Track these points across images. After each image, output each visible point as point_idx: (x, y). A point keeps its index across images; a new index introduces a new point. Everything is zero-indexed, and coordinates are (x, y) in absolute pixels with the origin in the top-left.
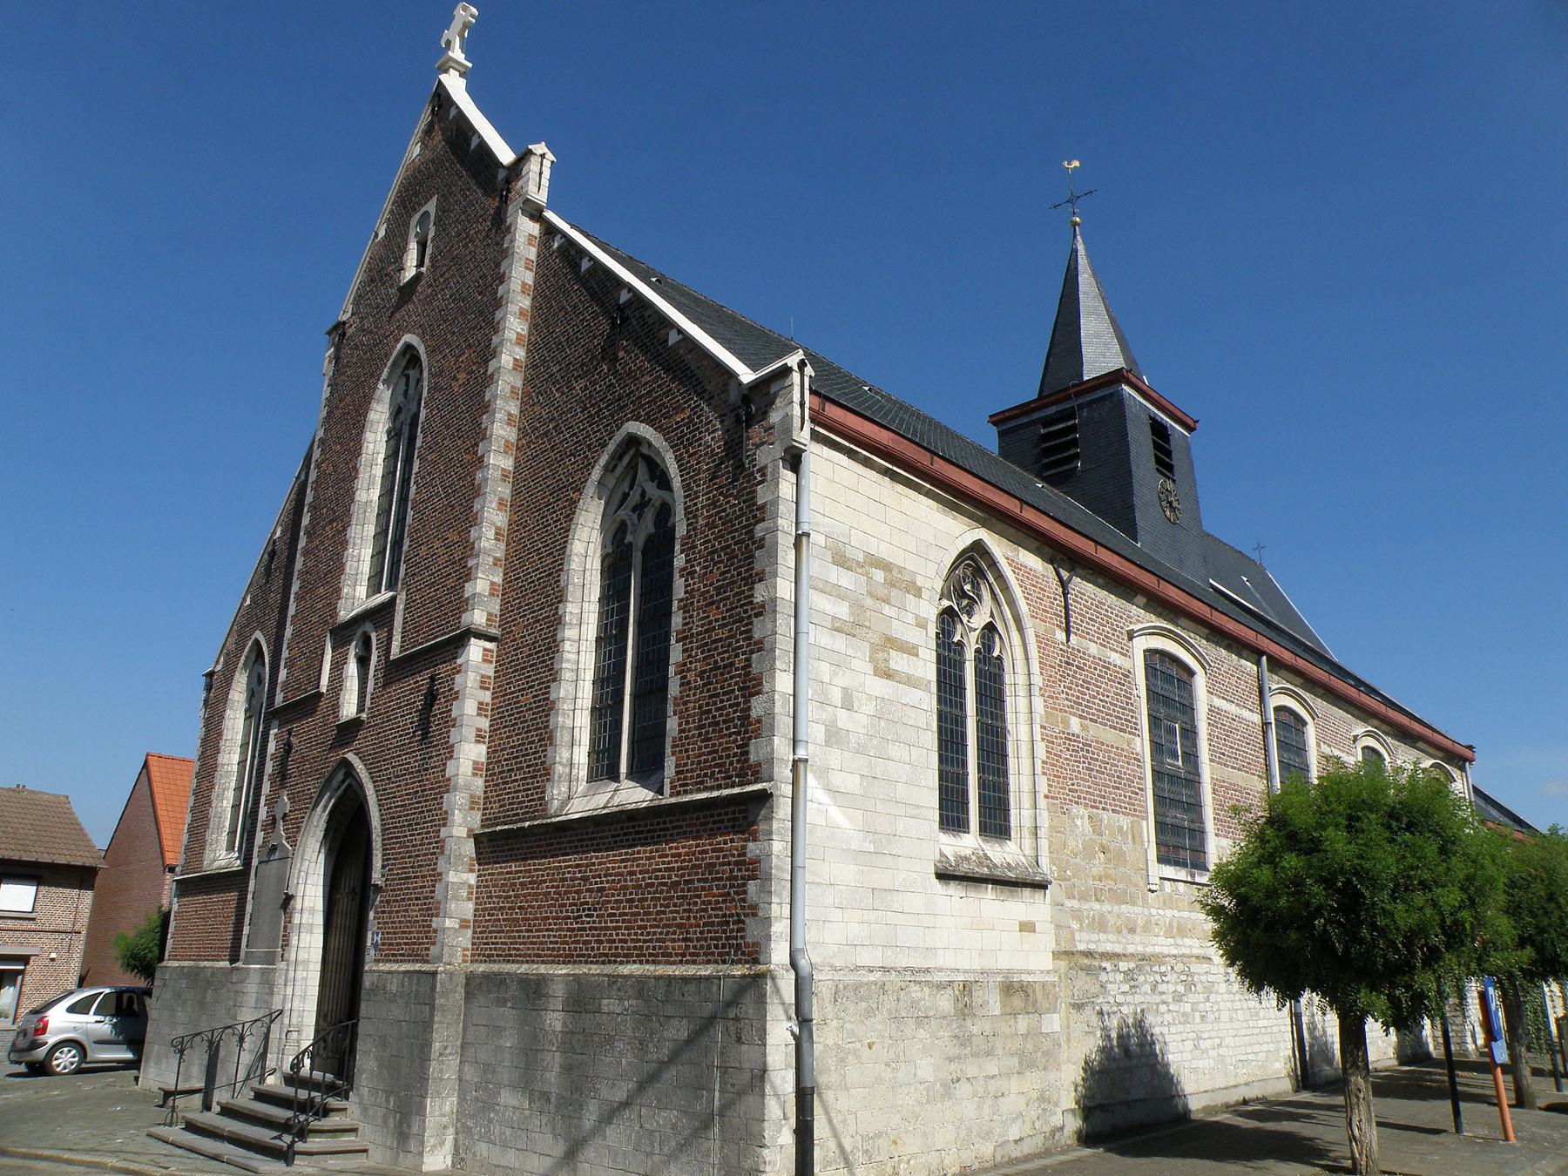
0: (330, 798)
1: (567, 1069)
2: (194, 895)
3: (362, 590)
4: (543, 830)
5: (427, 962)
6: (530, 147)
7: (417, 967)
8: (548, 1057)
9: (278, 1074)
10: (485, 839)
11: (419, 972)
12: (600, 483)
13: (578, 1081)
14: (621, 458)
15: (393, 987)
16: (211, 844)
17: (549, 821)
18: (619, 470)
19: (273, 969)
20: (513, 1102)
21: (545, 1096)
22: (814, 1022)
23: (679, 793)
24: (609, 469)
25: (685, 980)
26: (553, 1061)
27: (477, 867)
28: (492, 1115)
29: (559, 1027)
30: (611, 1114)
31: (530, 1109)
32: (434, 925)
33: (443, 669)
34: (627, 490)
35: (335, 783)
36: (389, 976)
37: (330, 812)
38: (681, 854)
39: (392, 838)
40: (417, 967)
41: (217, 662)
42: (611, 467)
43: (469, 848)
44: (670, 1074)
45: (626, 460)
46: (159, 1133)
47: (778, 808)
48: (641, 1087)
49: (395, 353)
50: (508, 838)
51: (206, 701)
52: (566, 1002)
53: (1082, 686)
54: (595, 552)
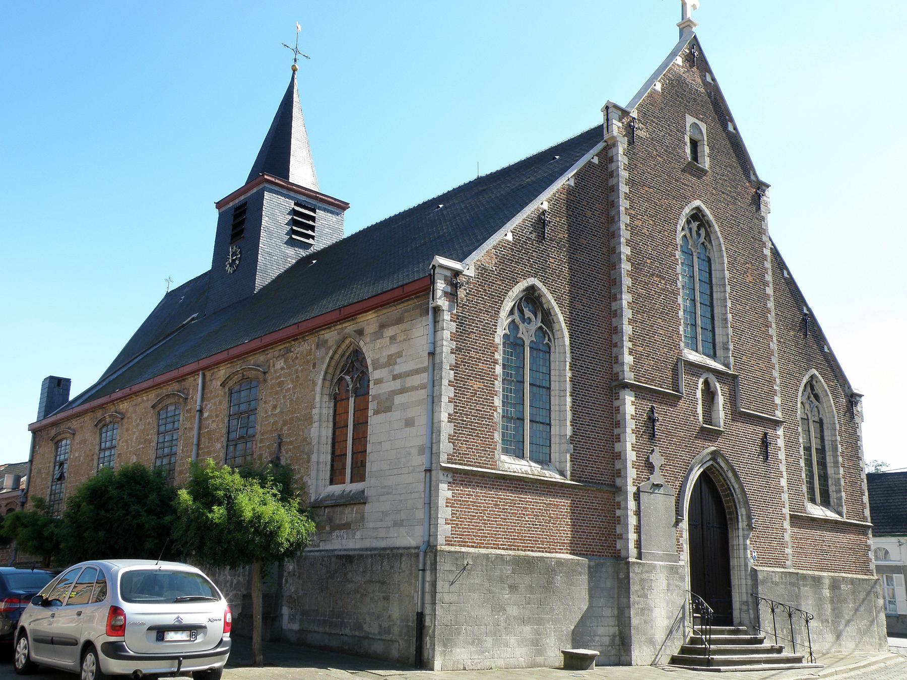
1: (833, 609)
2: (541, 495)
4: (806, 518)
5: (786, 568)
8: (826, 606)
13: (837, 614)
15: (776, 579)
20: (816, 625)
23: (848, 519)
25: (863, 580)
26: (828, 607)
30: (848, 622)
31: (822, 626)
32: (786, 552)
36: (774, 574)
39: (755, 505)
44: (862, 609)
48: (855, 613)
52: (830, 586)
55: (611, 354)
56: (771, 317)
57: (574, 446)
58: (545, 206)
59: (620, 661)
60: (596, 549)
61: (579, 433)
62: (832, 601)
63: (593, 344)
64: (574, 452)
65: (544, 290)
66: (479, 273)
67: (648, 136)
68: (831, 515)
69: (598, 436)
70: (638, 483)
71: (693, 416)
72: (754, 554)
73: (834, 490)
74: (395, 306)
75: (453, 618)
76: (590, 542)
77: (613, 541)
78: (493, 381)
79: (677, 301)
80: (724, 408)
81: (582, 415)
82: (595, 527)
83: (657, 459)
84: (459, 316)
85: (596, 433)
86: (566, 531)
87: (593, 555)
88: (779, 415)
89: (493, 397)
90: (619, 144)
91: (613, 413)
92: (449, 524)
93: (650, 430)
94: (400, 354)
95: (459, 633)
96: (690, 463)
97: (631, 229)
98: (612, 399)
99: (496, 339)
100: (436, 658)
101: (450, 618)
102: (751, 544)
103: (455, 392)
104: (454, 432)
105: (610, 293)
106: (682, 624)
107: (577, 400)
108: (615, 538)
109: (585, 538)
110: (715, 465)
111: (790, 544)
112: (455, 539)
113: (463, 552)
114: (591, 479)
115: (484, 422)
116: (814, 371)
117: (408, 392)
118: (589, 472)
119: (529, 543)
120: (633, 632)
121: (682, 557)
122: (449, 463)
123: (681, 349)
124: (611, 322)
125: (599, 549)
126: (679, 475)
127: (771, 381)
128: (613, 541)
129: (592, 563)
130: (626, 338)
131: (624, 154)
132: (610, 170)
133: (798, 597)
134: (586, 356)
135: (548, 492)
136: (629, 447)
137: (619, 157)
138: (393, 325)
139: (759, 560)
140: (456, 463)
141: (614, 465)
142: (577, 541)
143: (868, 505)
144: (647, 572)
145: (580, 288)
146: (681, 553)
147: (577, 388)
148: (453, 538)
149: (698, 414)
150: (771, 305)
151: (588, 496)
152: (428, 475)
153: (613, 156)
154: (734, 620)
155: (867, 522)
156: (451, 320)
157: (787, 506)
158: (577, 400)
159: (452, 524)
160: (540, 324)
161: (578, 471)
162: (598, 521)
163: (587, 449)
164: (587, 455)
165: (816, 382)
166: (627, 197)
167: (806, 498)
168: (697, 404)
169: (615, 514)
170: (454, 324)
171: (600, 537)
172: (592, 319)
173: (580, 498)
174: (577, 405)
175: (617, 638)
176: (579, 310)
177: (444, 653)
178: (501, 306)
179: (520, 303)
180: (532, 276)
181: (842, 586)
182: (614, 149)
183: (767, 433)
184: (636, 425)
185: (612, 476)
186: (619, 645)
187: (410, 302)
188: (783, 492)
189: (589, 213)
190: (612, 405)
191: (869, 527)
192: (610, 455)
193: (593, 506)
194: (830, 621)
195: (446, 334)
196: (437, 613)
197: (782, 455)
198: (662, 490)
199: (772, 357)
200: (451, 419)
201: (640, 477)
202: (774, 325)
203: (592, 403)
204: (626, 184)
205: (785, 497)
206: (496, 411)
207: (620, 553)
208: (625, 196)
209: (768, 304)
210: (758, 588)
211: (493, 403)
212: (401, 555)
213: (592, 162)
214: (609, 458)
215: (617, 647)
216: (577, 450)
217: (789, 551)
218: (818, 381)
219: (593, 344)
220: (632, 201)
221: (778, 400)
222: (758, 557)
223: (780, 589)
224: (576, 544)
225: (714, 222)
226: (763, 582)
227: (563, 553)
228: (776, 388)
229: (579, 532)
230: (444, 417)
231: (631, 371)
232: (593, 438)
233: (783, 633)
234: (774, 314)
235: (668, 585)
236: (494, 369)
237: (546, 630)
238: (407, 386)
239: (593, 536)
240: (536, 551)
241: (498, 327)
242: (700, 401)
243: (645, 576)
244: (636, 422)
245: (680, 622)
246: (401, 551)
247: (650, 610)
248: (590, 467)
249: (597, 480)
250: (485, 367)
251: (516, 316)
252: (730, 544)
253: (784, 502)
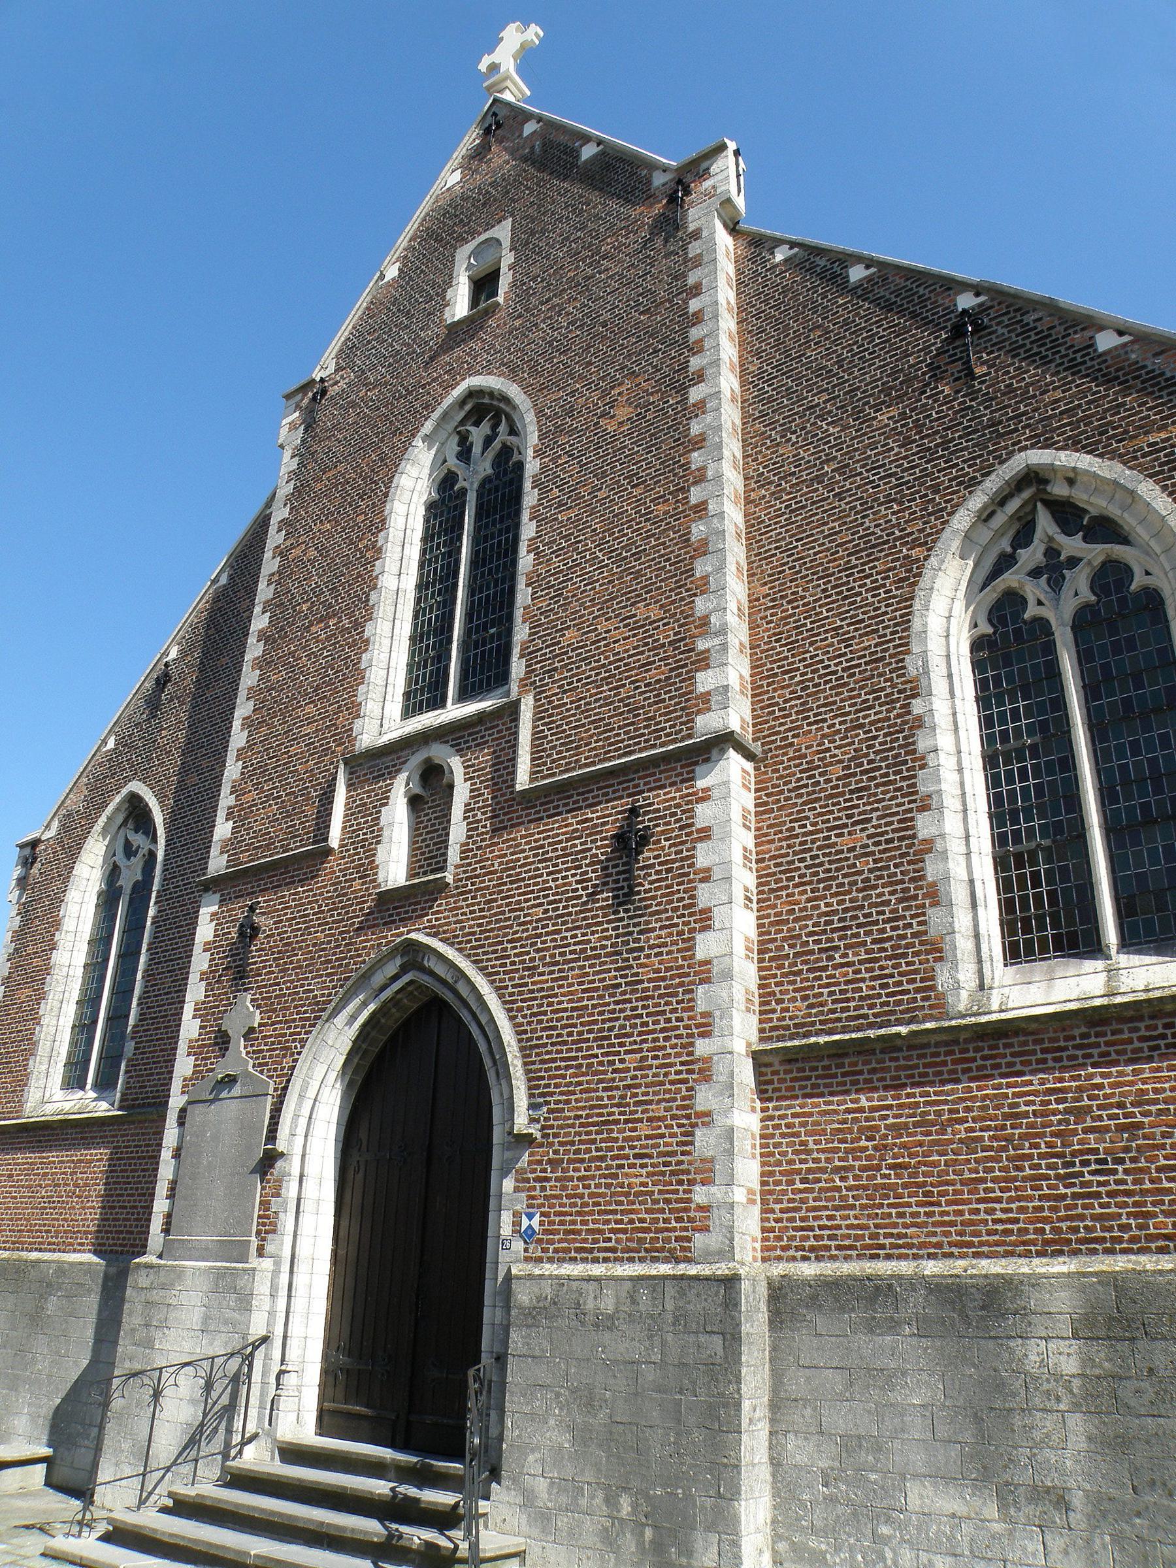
0: (365, 1004)
3: (395, 707)
5: (688, 1260)
6: (726, 140)
7: (664, 1269)
9: (263, 1443)
10: (775, 1060)
11: (682, 1277)
12: (967, 537)
14: (1002, 503)
16: (38, 1079)
17: (953, 1023)
18: (1000, 519)
19: (244, 1270)
24: (985, 517)
27: (758, 1104)
28: (885, 1530)
33: (658, 799)
34: (1009, 549)
35: (379, 979)
36: (592, 1286)
37: (364, 1026)
38: (918, 1103)
40: (664, 1269)
41: (48, 827)
42: (984, 516)
43: (745, 1073)
45: (1013, 505)
46: (85, 1554)
49: (447, 402)
50: (846, 1055)
51: (22, 882)
54: (960, 631)
72: (525, 1222)
102: (517, 1190)
106: (224, 1424)
110: (425, 979)
129: (113, 1270)
135: (82, 1138)
144: (163, 1287)
146: (269, 1237)
194: (1077, 1499)
196: (509, 1379)
198: (237, 1090)
214: (534, 1031)
222: (546, 1232)
224: (106, 1232)
235: (206, 1318)
240: (45, 1250)
243: (155, 1296)
245: (221, 1418)
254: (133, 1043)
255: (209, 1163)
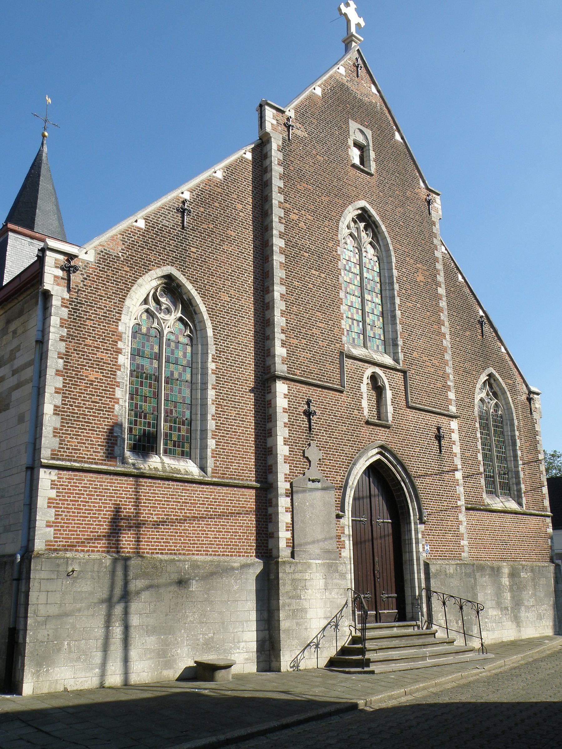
1: (513, 597)
6: (349, 1)
21: (506, 608)
22: (147, 638)
26: (508, 596)
28: (486, 620)
29: (508, 583)
32: (462, 544)
47: (170, 458)
53: (369, 436)
55: (264, 348)
56: (444, 316)
57: (216, 441)
58: (187, 196)
59: (270, 667)
60: (243, 549)
61: (224, 427)
62: (511, 590)
63: (242, 336)
64: (216, 448)
65: (183, 279)
66: (100, 258)
67: (307, 135)
68: (512, 505)
69: (246, 431)
70: (291, 478)
71: (357, 410)
72: (426, 548)
73: (514, 482)
74: (16, 298)
75: (51, 632)
76: (235, 542)
77: (264, 540)
78: (115, 372)
79: (338, 296)
80: (392, 402)
81: (228, 409)
82: (242, 526)
83: (314, 453)
84: (73, 301)
85: (245, 427)
86: (205, 531)
87: (239, 556)
88: (453, 409)
89: (114, 389)
90: (273, 140)
91: (265, 407)
92: (50, 526)
93: (306, 424)
94: (18, 348)
95: (59, 650)
96: (353, 458)
97: (286, 222)
98: (264, 393)
99: (120, 328)
100: (25, 680)
101: (47, 633)
102: (422, 537)
103: (64, 383)
104: (62, 426)
105: (264, 286)
107: (222, 393)
108: (266, 537)
109: (229, 538)
111: (466, 536)
112: (59, 543)
113: (67, 558)
114: (237, 475)
115: (102, 415)
116: (491, 370)
117: (22, 386)
118: (235, 469)
119: (158, 546)
120: (282, 636)
121: (343, 554)
122: (53, 459)
123: (343, 342)
124: (264, 315)
125: (247, 549)
126: (340, 470)
127: (445, 377)
128: (264, 540)
130: (277, 330)
131: (278, 150)
132: (264, 167)
133: (473, 588)
134: (233, 348)
136: (280, 441)
137: (273, 152)
138: (16, 319)
139: (432, 553)
140: (63, 460)
141: (266, 461)
142: (220, 541)
143: (547, 495)
145: (226, 280)
146: (343, 550)
147: (222, 381)
148: (56, 542)
149: (363, 408)
150: (443, 304)
151: (233, 494)
152: (29, 472)
153: (267, 153)
154: (407, 614)
155: (546, 511)
156: (62, 306)
157: (462, 498)
158: (222, 393)
159: (55, 526)
160: (179, 315)
161: (221, 467)
162: (245, 520)
163: (232, 444)
164: (233, 450)
165: (494, 380)
166: (281, 191)
167: (485, 491)
168: (362, 398)
169: (267, 512)
170: (66, 310)
171: (248, 536)
172: (241, 311)
173: (223, 496)
174: (221, 399)
175: (267, 643)
176: (225, 301)
177: (37, 674)
178: (127, 294)
179: (155, 294)
180: (168, 264)
181: (522, 574)
182: (268, 146)
183: (440, 428)
184: (289, 418)
185: (264, 472)
186: (269, 650)
187: (28, 292)
188: (458, 485)
189: (240, 207)
190: (265, 399)
191: (548, 516)
192: (262, 451)
193: (239, 504)
194: (509, 608)
195: (54, 320)
197: (456, 449)
199: (445, 354)
200: (57, 411)
201: (293, 472)
202: (447, 324)
203: (240, 396)
204: (280, 179)
205: (460, 490)
206: (118, 403)
207: (271, 553)
208: (279, 190)
209: (440, 304)
210: (430, 581)
211: (114, 395)
212: (6, 563)
213: (244, 158)
215: (267, 652)
216: (220, 445)
217: (464, 543)
218: (496, 380)
219: (242, 336)
220: (286, 195)
221: (452, 395)
222: (431, 551)
223: (455, 582)
225: (381, 223)
226: (436, 575)
227: (201, 555)
228: (449, 383)
229: (221, 532)
230: (48, 409)
231: (283, 363)
232: (240, 433)
233: (455, 625)
234: (446, 314)
235: (326, 584)
236: (117, 359)
237: (176, 639)
238: (21, 380)
239: (240, 536)
241: (123, 316)
242: (365, 396)
243: (297, 576)
244: (289, 415)
246: (5, 559)
247: (304, 610)
248: (237, 463)
249: (245, 476)
250: (105, 356)
251: (152, 305)
252: (402, 538)
253: (459, 495)
254: (214, 441)
255: (310, 517)
